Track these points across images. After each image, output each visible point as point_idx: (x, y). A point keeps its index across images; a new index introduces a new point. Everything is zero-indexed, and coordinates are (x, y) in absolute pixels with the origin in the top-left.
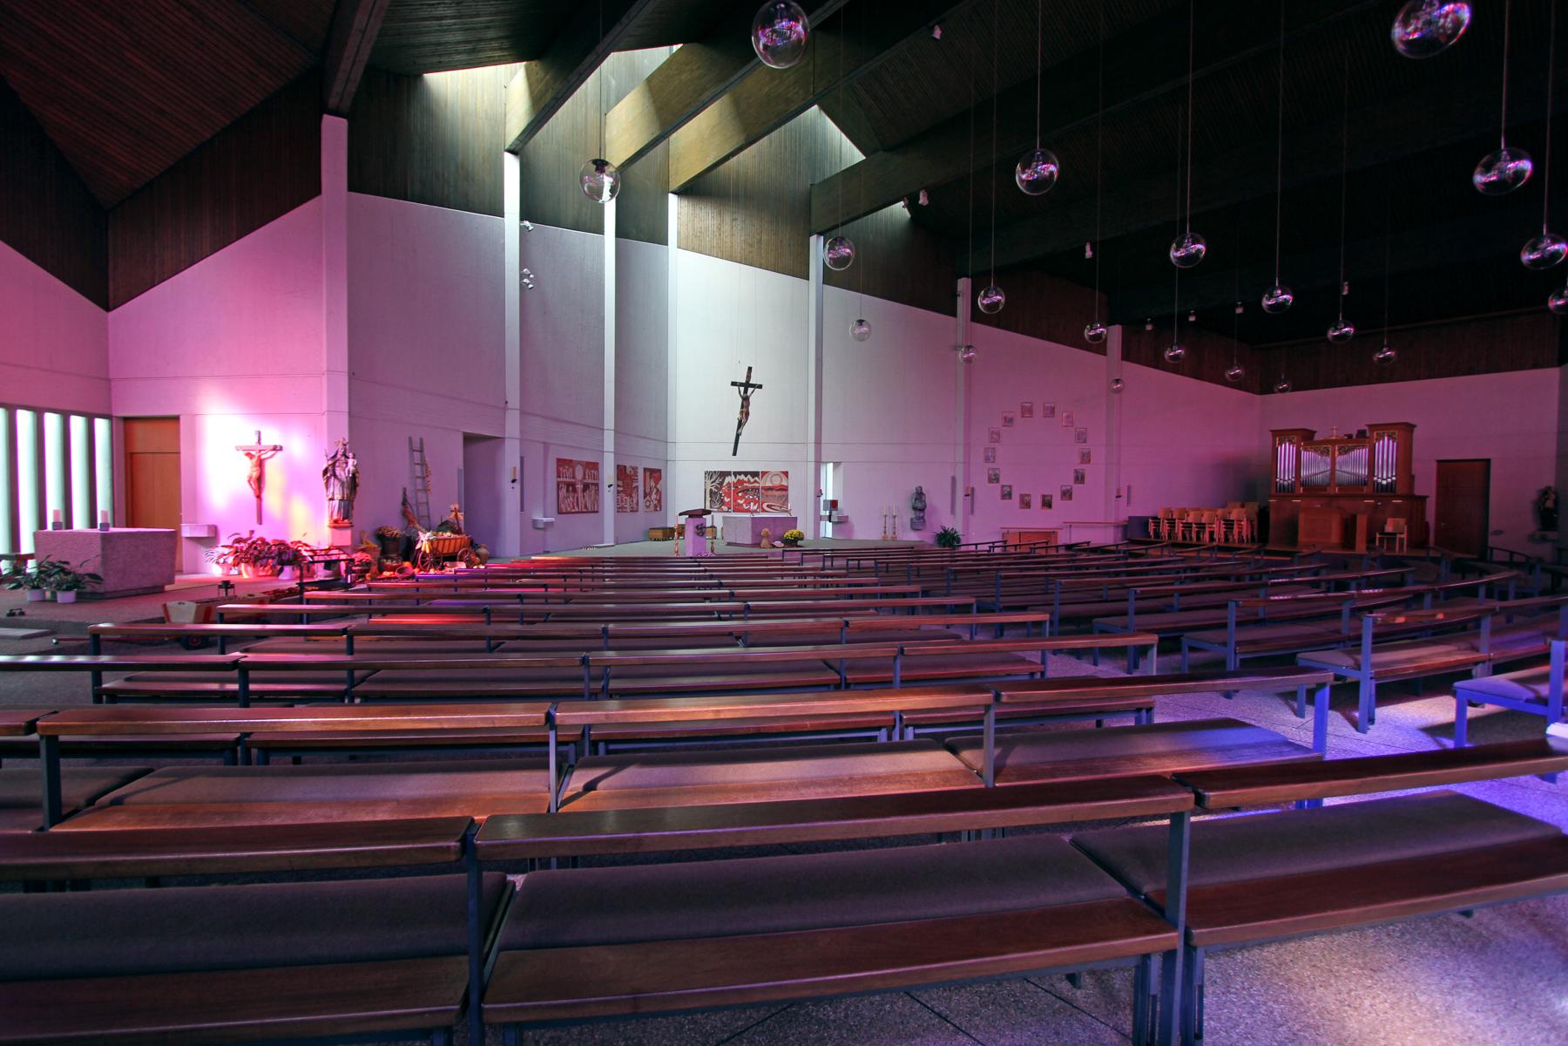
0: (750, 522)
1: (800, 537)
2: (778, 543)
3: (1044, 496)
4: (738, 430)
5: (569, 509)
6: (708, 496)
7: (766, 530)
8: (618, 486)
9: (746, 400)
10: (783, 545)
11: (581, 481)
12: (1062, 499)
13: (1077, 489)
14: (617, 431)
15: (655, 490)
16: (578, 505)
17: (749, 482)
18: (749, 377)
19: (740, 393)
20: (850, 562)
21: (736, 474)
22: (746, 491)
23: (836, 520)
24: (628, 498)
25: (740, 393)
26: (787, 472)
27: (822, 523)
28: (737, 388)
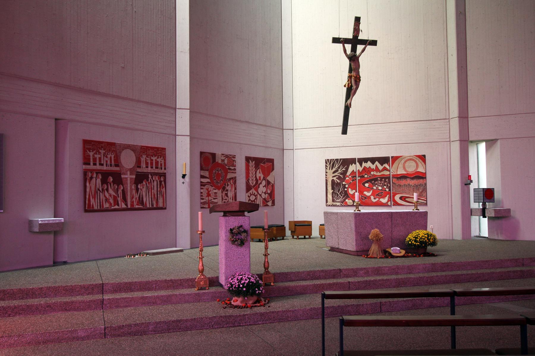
0: (353, 216)
1: (431, 241)
2: (395, 250)
4: (346, 101)
5: (106, 205)
6: (330, 188)
7: (376, 231)
8: (202, 177)
9: (354, 59)
10: (403, 252)
11: (132, 171)
14: (193, 112)
15: (264, 183)
16: (125, 199)
17: (377, 169)
18: (357, 30)
19: (345, 51)
20: (327, 301)
21: (361, 161)
22: (373, 180)
23: (493, 215)
24: (219, 192)
25: (345, 51)
26: (424, 156)
27: (474, 219)
28: (341, 45)
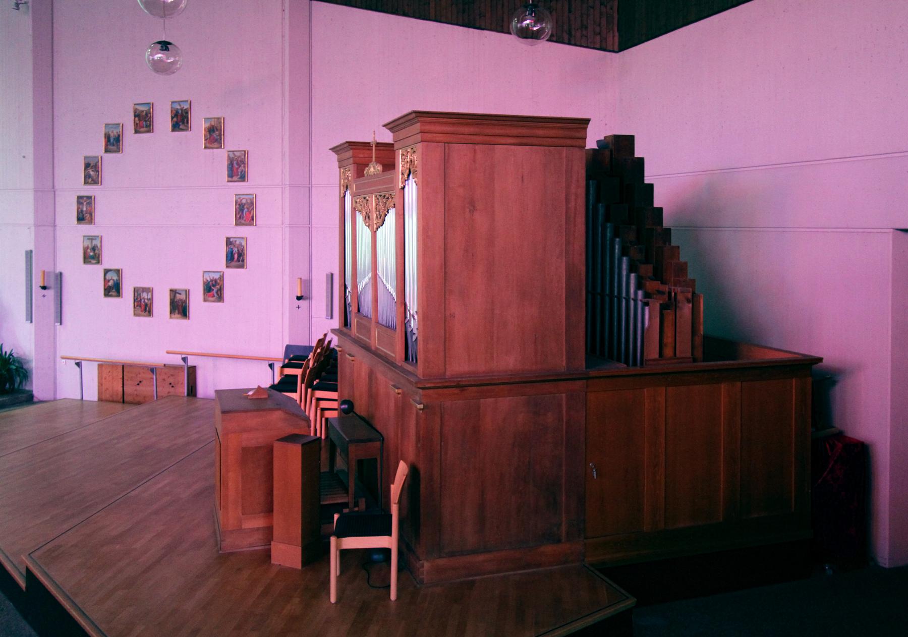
3: (173, 292)
12: (205, 300)
13: (233, 278)
26: (105, 270)
